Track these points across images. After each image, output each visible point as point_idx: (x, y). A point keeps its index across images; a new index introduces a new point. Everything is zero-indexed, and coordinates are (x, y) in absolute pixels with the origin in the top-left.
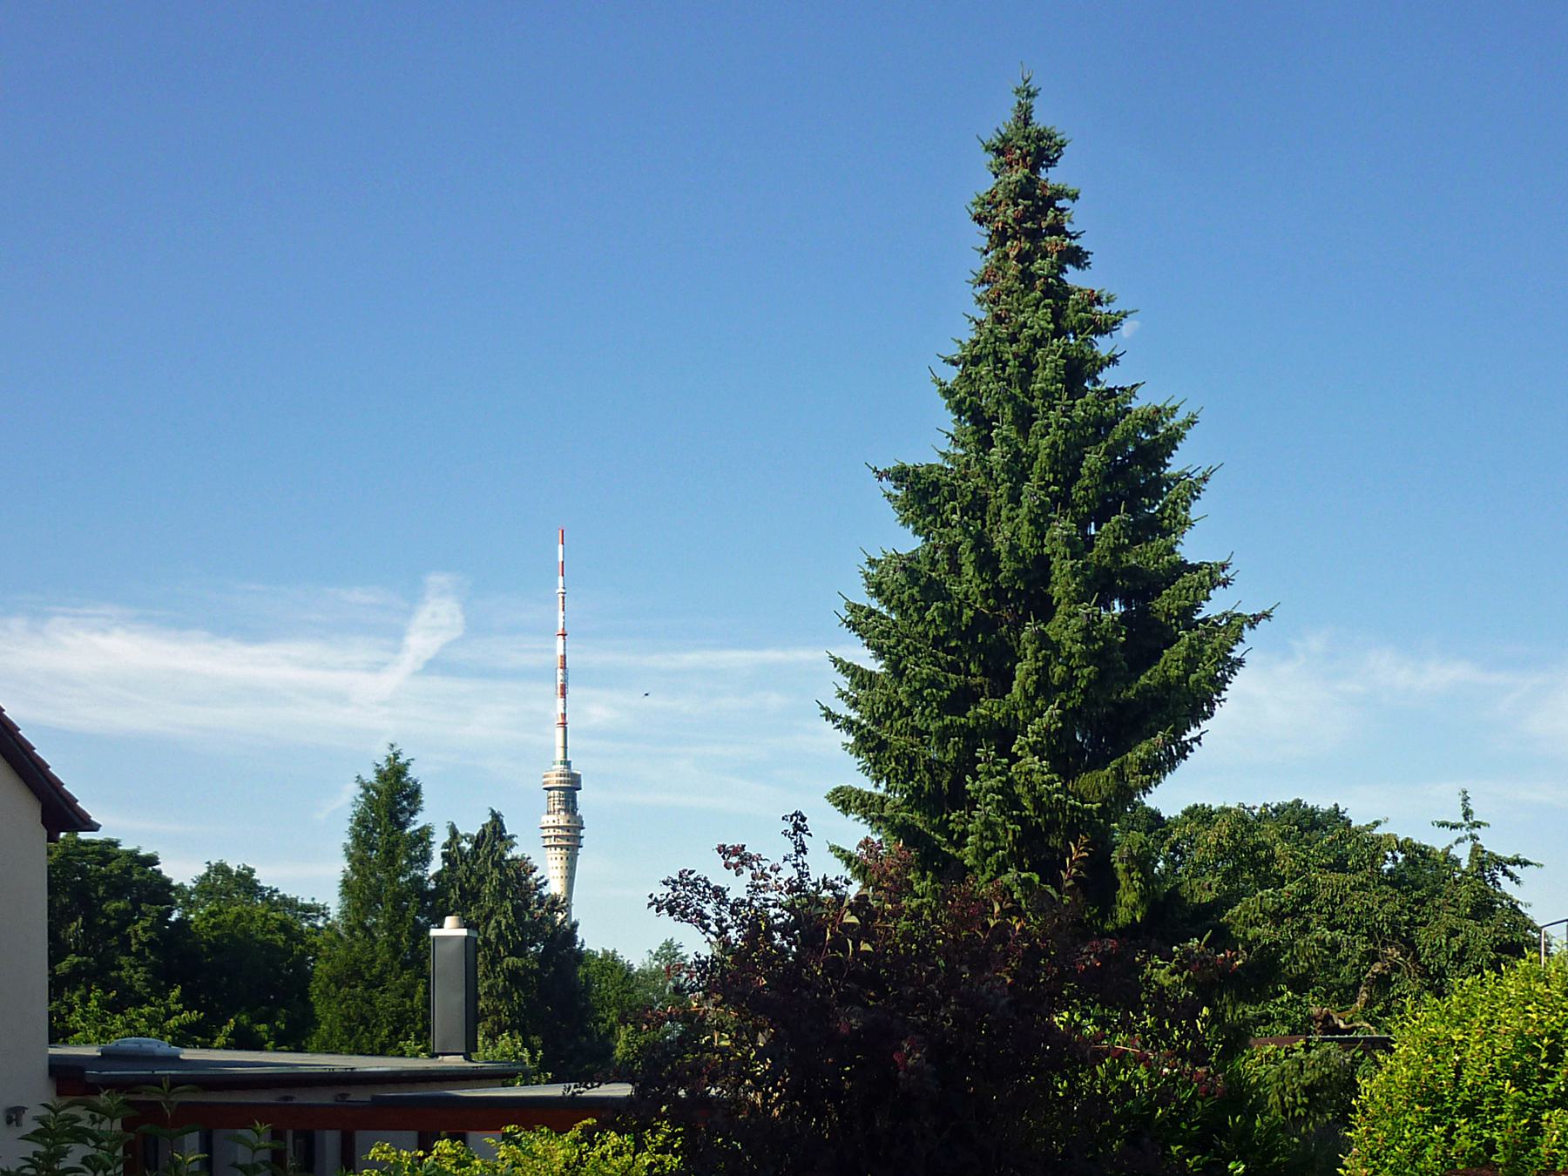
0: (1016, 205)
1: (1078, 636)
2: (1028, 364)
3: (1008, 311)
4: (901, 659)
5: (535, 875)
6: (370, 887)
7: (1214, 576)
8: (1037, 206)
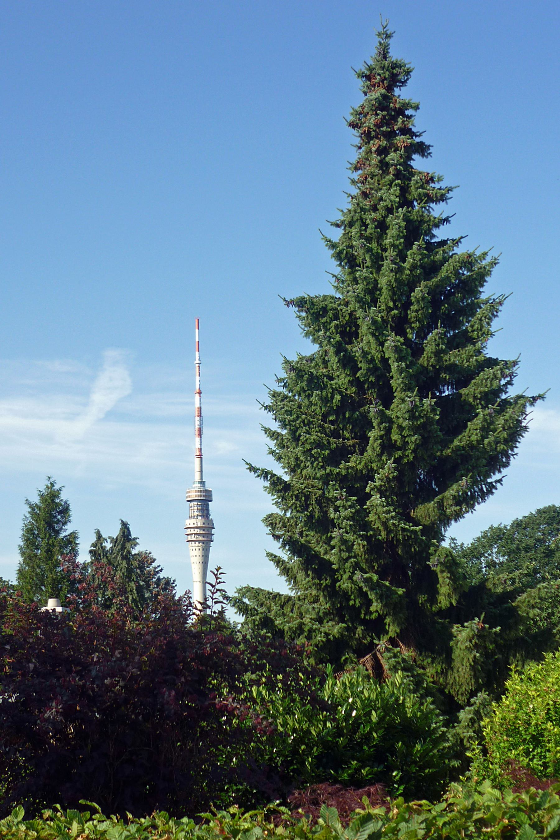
0: (377, 115)
1: (407, 416)
2: (382, 226)
3: (372, 189)
4: (297, 429)
5: (154, 565)
6: (37, 574)
7: (507, 368)
8: (391, 115)
